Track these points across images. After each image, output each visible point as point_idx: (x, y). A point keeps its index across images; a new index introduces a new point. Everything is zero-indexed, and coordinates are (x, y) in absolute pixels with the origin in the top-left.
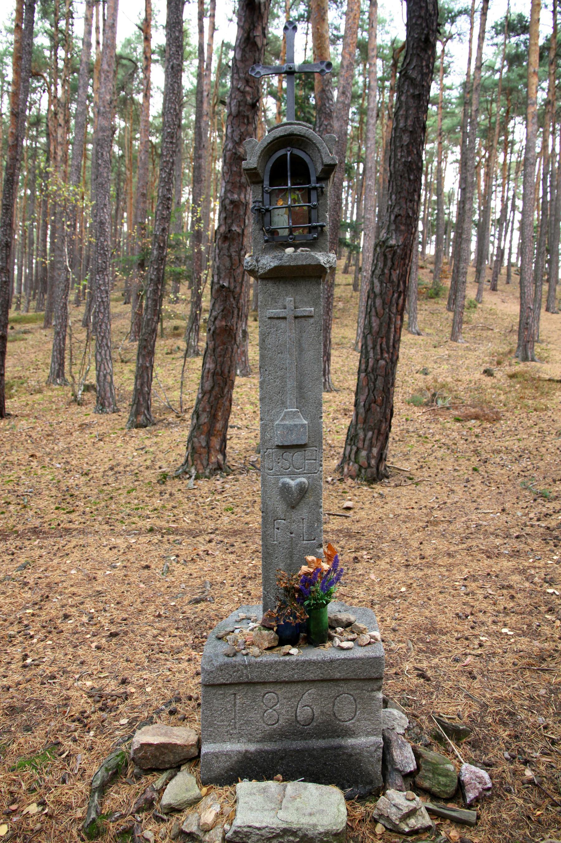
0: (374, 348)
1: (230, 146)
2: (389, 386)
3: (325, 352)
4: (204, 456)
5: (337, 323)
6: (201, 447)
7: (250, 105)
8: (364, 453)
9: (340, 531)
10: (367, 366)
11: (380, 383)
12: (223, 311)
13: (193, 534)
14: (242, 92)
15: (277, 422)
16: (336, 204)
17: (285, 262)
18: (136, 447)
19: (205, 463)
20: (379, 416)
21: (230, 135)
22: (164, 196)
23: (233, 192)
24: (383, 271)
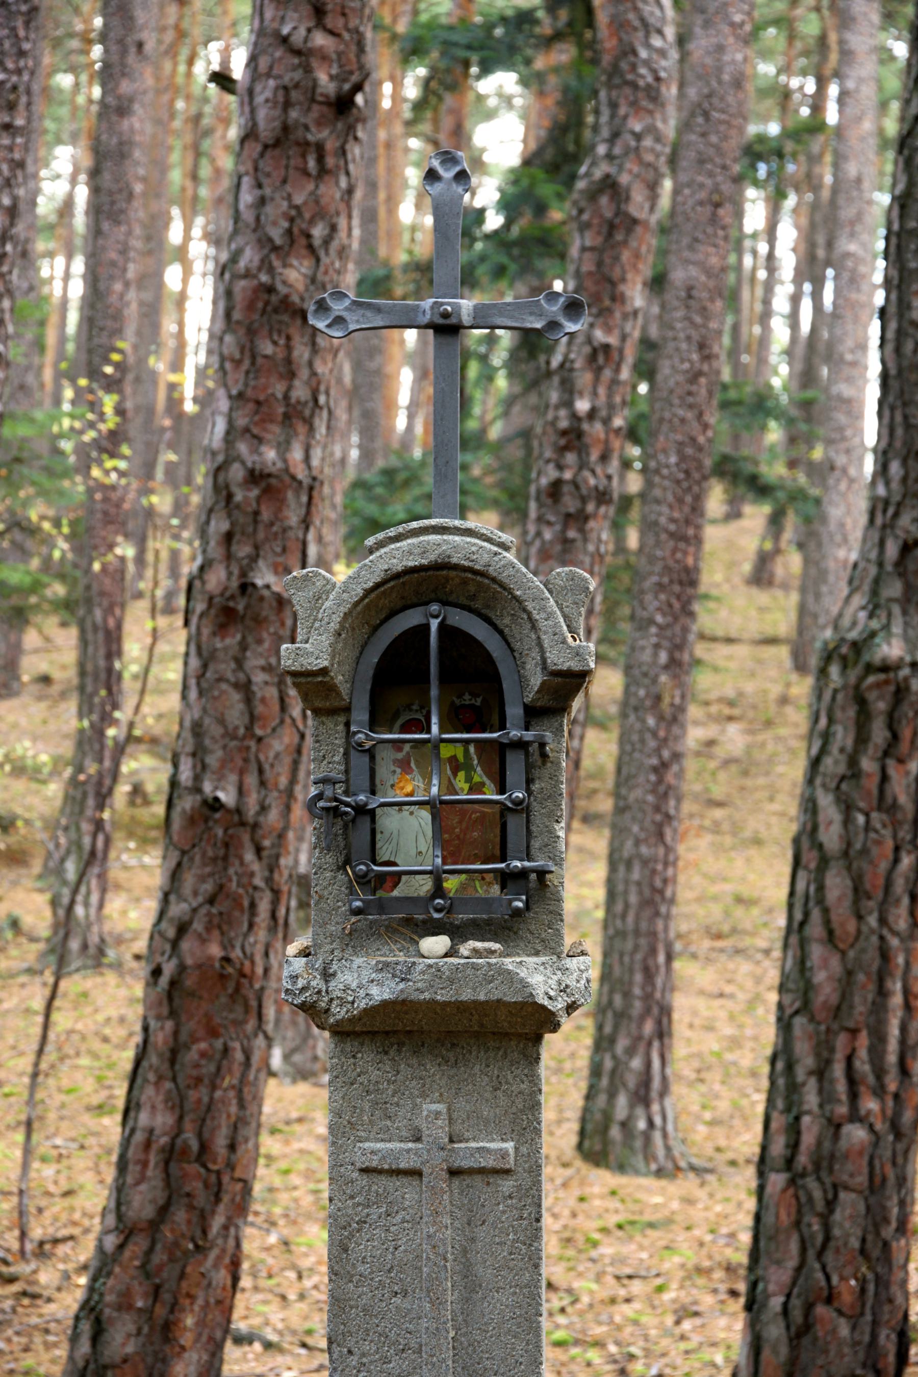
0: (821, 1073)
1: (250, 257)
2: (888, 1232)
3: (648, 997)
5: (716, 828)
7: (328, 104)
10: (794, 1146)
11: (848, 1214)
12: (211, 901)
14: (298, 53)
17: (418, 988)
21: (248, 216)
23: (260, 440)
24: (853, 762)
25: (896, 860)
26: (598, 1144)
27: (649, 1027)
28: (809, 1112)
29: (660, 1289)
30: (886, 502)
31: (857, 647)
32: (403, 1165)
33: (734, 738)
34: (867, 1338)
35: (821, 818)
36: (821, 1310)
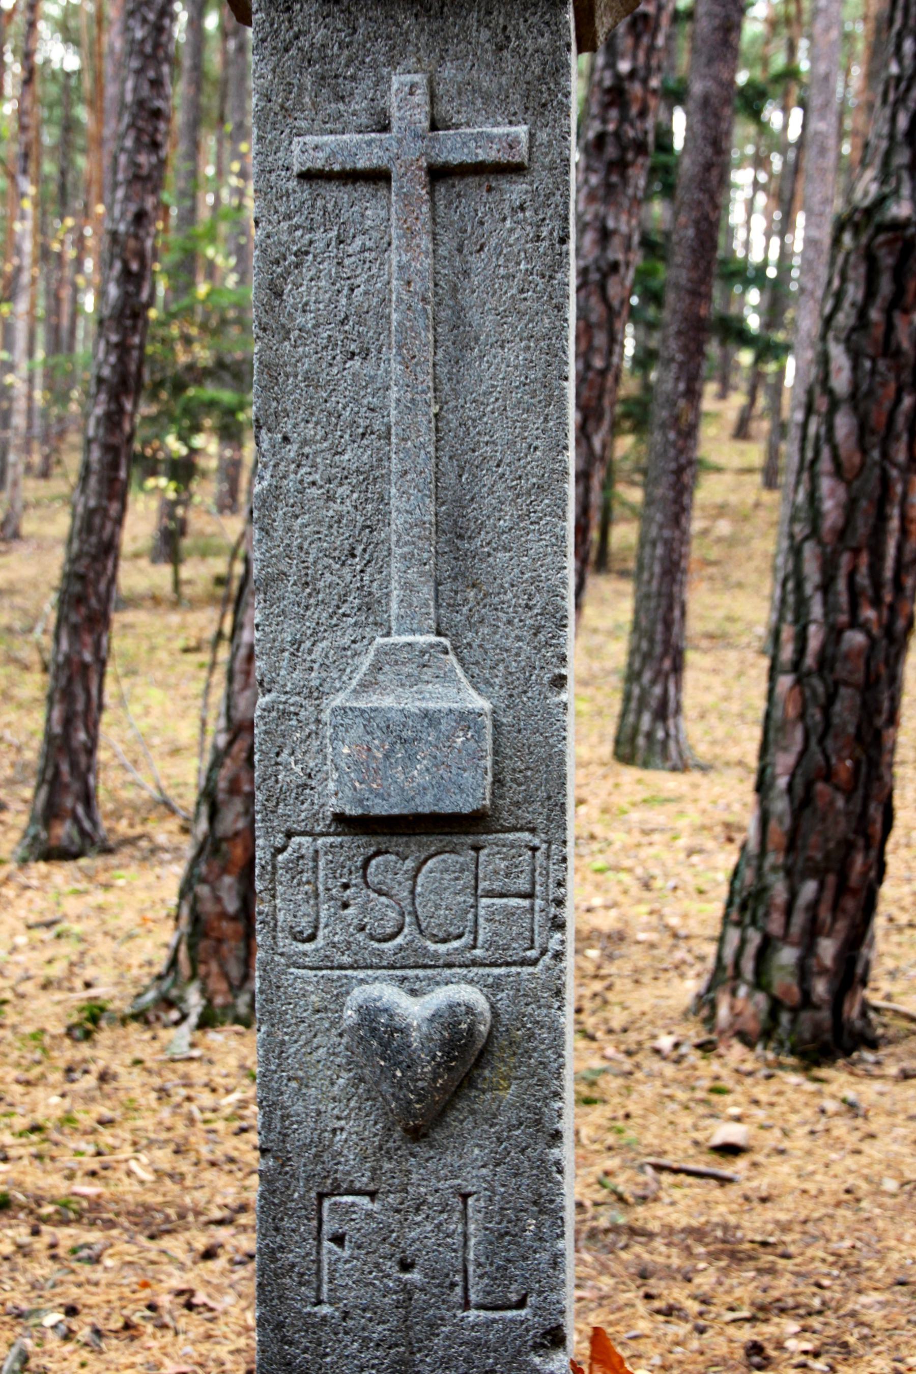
0: (826, 587)
2: (881, 720)
3: (667, 642)
4: (232, 948)
5: (711, 578)
6: (223, 915)
8: (787, 956)
9: (698, 1233)
13: (152, 1223)
15: (338, 700)
16: (708, 167)
18: (33, 919)
19: (235, 971)
20: (841, 828)
22: (141, 103)
24: (862, 313)
25: (898, 401)
26: (629, 749)
27: (667, 664)
28: (815, 621)
29: (675, 838)
30: (899, 79)
31: (869, 212)
32: (361, 164)
33: (724, 527)
34: (858, 809)
35: (833, 366)
36: (820, 786)
